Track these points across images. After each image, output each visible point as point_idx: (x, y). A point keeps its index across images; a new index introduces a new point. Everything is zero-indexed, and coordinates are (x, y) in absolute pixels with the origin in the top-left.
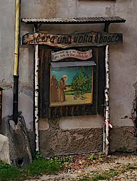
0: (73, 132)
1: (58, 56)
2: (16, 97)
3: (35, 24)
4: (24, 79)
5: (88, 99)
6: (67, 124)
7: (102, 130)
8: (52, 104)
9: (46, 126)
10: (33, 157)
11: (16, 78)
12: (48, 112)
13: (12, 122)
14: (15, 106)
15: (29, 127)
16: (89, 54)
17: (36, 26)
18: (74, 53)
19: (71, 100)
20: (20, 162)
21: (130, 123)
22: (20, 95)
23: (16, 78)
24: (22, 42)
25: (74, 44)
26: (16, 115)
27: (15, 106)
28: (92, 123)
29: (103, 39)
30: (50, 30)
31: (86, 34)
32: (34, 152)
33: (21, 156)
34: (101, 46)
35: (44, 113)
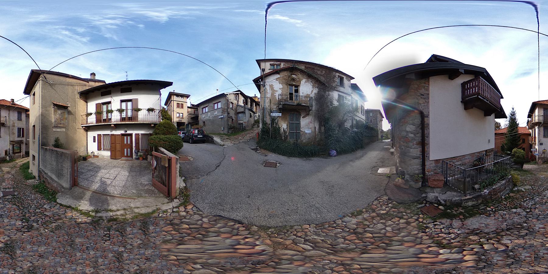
6: (16, 154)
12: (14, 153)
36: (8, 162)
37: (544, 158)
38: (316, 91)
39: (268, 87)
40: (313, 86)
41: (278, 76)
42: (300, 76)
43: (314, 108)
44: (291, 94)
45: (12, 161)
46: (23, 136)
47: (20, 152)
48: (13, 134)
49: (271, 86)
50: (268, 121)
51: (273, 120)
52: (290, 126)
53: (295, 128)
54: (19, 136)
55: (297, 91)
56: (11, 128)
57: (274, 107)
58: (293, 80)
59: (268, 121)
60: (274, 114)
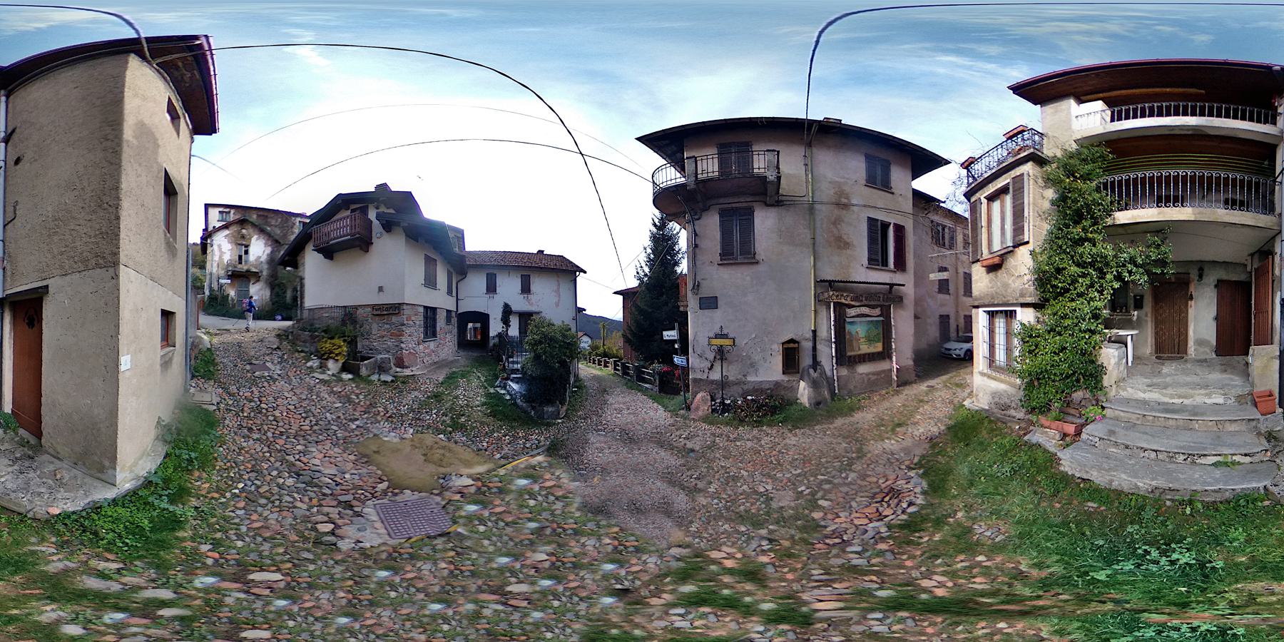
0: (867, 374)
1: (851, 312)
2: (814, 348)
3: (830, 282)
4: (823, 333)
5: (879, 347)
6: (863, 369)
7: (891, 370)
8: (849, 354)
9: (844, 372)
10: (833, 399)
11: (814, 332)
12: (845, 358)
13: (811, 371)
14: (814, 357)
15: (829, 373)
16: (878, 311)
17: (831, 283)
18: (865, 310)
19: (865, 349)
20: (818, 403)
21: (911, 363)
22: (819, 347)
23: (814, 332)
24: (818, 300)
25: (865, 302)
26: (816, 364)
27: (814, 357)
28: (883, 366)
29: (888, 299)
30: (845, 290)
31: (876, 294)
32: (833, 394)
33: (819, 399)
34: (718, 235)
35: (366, 596)
36: (802, 419)
37: (723, 384)
38: (269, 250)
39: (215, 247)
40: (266, 244)
41: (227, 232)
42: (251, 230)
43: (265, 273)
44: (240, 257)
45: (831, 415)
46: (901, 265)
47: (885, 354)
48: (842, 244)
49: (219, 246)
50: (215, 286)
51: (221, 286)
52: (239, 293)
53: (245, 294)
54: (877, 259)
55: (246, 252)
56: (823, 211)
57: (222, 273)
58: (243, 237)
59: (215, 286)
60: (222, 281)
